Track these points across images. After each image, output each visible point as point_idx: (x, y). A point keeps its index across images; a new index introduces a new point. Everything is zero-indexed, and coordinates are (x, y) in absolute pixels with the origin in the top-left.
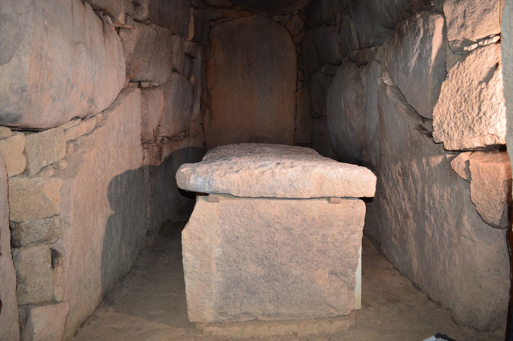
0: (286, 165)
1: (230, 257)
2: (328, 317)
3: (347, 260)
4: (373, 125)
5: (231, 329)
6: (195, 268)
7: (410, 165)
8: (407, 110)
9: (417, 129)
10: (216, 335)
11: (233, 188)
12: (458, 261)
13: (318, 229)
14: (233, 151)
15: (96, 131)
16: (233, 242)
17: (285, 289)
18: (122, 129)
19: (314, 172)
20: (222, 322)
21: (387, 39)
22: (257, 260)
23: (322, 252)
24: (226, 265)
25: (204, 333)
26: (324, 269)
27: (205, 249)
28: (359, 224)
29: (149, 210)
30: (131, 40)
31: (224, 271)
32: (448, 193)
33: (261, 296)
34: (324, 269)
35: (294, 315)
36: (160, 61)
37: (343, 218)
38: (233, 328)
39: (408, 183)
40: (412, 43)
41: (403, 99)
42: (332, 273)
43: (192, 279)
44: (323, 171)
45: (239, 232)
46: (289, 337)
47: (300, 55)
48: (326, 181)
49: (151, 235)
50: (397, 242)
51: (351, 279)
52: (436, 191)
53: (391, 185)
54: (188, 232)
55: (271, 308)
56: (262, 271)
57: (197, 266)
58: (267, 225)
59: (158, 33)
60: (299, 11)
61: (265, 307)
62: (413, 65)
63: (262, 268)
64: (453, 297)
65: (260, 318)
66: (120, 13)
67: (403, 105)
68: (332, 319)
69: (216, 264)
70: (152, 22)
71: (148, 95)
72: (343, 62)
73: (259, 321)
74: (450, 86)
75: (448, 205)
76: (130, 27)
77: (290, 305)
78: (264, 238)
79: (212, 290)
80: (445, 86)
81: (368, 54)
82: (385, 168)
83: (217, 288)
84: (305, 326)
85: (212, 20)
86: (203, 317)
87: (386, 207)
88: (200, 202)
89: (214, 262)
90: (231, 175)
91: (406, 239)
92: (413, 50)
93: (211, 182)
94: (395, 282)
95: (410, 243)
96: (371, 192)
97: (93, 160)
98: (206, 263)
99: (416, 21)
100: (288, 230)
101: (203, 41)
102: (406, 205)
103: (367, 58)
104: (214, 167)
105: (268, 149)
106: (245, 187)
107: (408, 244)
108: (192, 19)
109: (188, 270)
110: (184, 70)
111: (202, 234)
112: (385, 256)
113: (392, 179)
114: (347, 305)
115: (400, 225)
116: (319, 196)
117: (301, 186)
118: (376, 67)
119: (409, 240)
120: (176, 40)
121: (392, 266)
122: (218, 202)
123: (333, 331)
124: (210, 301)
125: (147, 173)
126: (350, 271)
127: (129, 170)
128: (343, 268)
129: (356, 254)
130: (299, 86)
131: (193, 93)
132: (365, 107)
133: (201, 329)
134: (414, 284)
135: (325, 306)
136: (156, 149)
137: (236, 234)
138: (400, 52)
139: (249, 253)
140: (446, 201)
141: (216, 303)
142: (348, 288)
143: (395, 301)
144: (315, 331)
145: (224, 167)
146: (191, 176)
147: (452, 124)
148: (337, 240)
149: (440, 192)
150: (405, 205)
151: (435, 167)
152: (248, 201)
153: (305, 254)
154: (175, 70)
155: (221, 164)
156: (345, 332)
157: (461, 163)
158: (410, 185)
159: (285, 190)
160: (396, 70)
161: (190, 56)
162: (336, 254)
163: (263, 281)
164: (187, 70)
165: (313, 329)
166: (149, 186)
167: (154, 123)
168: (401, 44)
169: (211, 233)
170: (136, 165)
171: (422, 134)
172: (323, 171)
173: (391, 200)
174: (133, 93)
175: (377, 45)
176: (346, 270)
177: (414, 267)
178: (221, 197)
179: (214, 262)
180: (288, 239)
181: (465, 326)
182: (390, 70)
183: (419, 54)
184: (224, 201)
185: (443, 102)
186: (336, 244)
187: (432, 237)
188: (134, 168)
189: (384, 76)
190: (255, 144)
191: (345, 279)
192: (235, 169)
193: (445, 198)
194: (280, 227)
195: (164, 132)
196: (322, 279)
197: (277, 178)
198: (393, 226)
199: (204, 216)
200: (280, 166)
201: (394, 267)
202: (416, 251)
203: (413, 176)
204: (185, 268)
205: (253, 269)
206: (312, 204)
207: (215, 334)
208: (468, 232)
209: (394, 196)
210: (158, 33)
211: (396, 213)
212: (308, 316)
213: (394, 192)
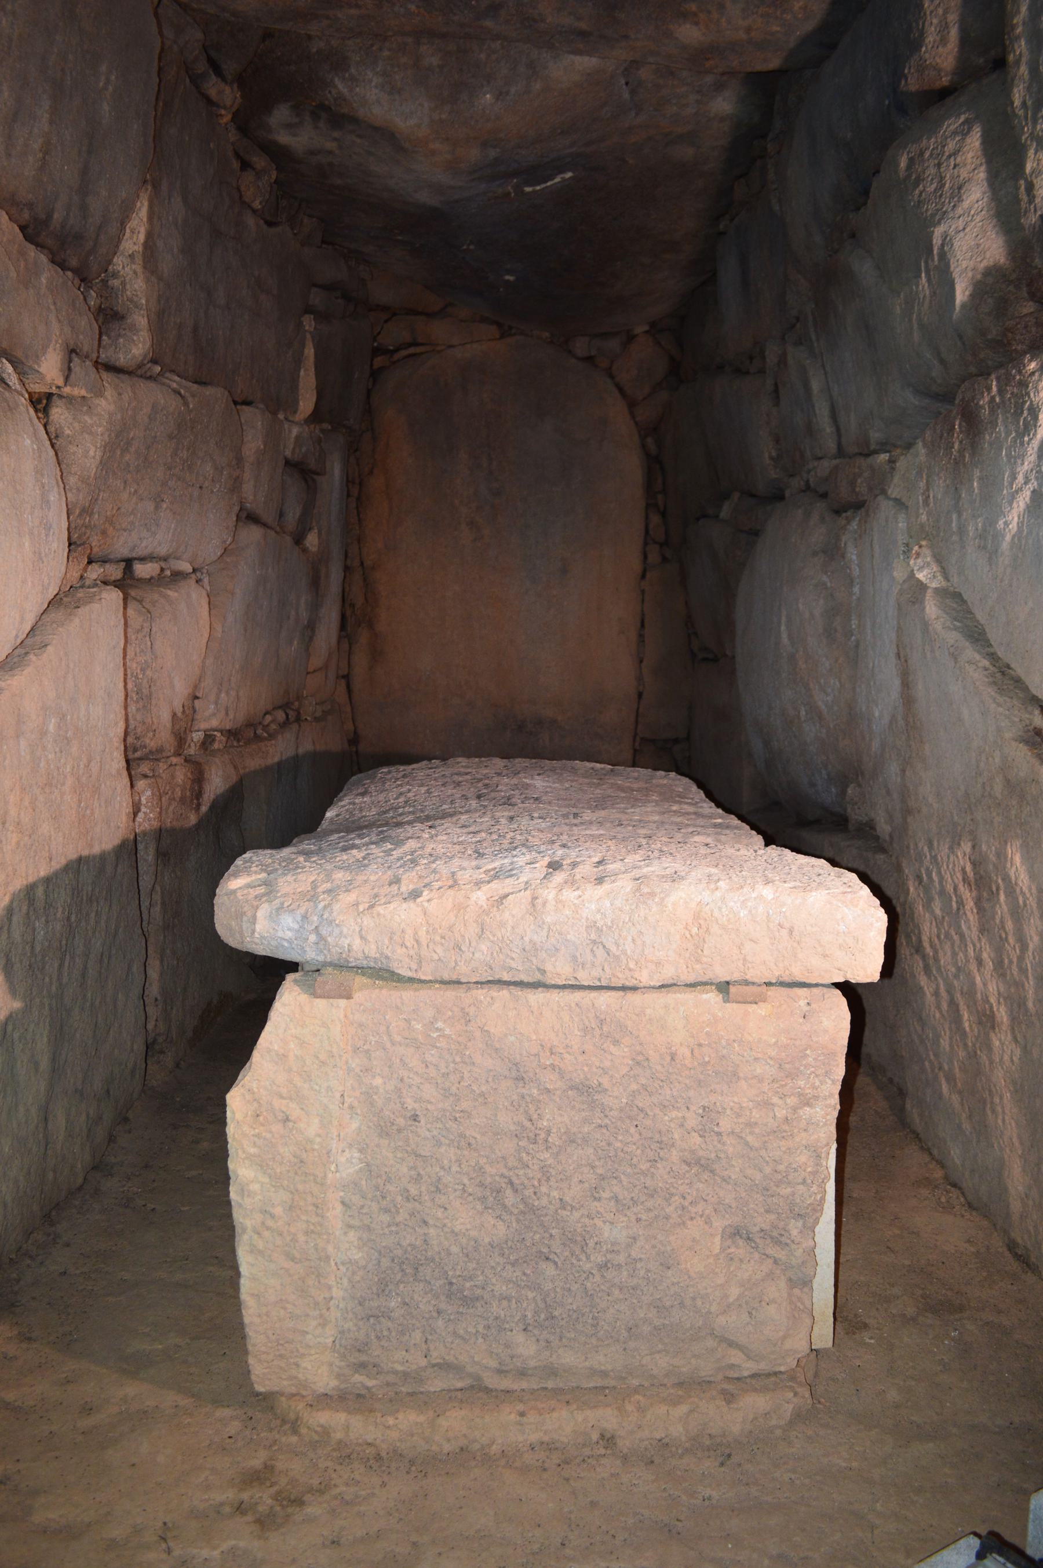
0: (580, 871)
1: (389, 1180)
2: (720, 1377)
3: (787, 1191)
4: (882, 706)
5: (391, 1421)
6: (272, 1216)
7: (1001, 855)
8: (993, 675)
9: (1026, 742)
10: (340, 1442)
11: (400, 951)
13: (688, 1088)
14: (423, 789)
16: (399, 1131)
17: (575, 1287)
18: (51, 728)
19: (672, 898)
20: (363, 1392)
21: (928, 434)
24: (374, 1206)
25: (303, 1431)
26: (708, 1222)
27: (304, 1155)
28: (827, 1074)
29: (154, 974)
30: (91, 433)
31: (369, 1229)
33: (495, 1309)
34: (708, 1222)
35: (604, 1374)
36: (196, 493)
38: (401, 1416)
39: (994, 913)
40: (1009, 456)
41: (978, 636)
42: (735, 1233)
43: (261, 1253)
45: (418, 1100)
46: (587, 1451)
47: (654, 464)
48: (715, 929)
49: (162, 1052)
50: (955, 1099)
51: (799, 1253)
53: (938, 912)
54: (248, 1097)
55: (527, 1348)
56: (496, 1229)
57: (278, 1211)
58: (514, 1074)
59: (186, 404)
60: (653, 325)
61: (507, 1346)
62: (1013, 526)
63: (499, 1217)
65: (492, 1381)
66: (45, 349)
67: (977, 657)
68: (732, 1387)
69: (343, 1203)
70: (167, 369)
71: (154, 603)
72: (787, 493)
73: (488, 1391)
76: (83, 393)
77: (594, 1341)
78: (506, 1120)
79: (330, 1288)
81: (866, 474)
82: (920, 857)
83: (345, 1281)
84: (641, 1410)
85: (377, 351)
86: (300, 1376)
87: (923, 980)
88: (289, 999)
89: (334, 1198)
90: (392, 906)
91: (986, 1095)
92: (1014, 477)
93: (324, 932)
94: (948, 1234)
95: (999, 1109)
96: (867, 968)
98: (309, 1199)
99: (1023, 384)
100: (585, 1091)
101: (350, 416)
102: (988, 985)
103: (862, 487)
104: (339, 876)
105: (539, 783)
106: (439, 950)
107: (993, 1111)
108: (310, 351)
109: (248, 1223)
110: (281, 515)
111: (295, 1103)
112: (917, 1136)
113: (942, 892)
114: (784, 1338)
115: (965, 1045)
116: (691, 979)
117: (629, 947)
118: (890, 523)
119: (997, 1100)
120: (254, 423)
121: (938, 1174)
122: (349, 997)
123: (736, 1429)
125: (148, 855)
126: (795, 1228)
127: (80, 859)
128: (773, 1217)
129: (814, 1173)
130: (650, 559)
131: (316, 583)
132: (857, 646)
133: (292, 1416)
134: (1012, 1246)
135: (710, 1343)
136: (181, 775)
137: (410, 1104)
138: (971, 481)
139: (455, 1168)
141: (342, 1332)
142: (790, 1280)
143: (944, 1307)
144: (677, 1431)
145: (373, 878)
146: (263, 903)
148: (750, 1125)
150: (985, 985)
152: (450, 994)
153: (644, 1174)
154: (249, 517)
155: (361, 865)
158: (1002, 922)
159: (574, 958)
160: (955, 538)
161: (303, 471)
162: (749, 1172)
163: (502, 1260)
164: (293, 514)
165: (671, 1421)
166: (157, 897)
167: (174, 692)
168: (973, 455)
170: (106, 838)
172: (706, 896)
173: (936, 960)
174: (96, 606)
175: (895, 446)
176: (781, 1224)
177: (1012, 1191)
178: (360, 980)
179: (334, 1198)
180: (585, 1121)
182: (935, 537)
183: (1034, 492)
184: (367, 995)
186: (750, 1138)
188: (96, 850)
189: (918, 555)
190: (499, 763)
192: (406, 887)
194: (559, 1084)
195: (212, 717)
196: (701, 1258)
197: (548, 919)
198: (945, 1043)
200: (559, 877)
201: (946, 1177)
202: (1020, 1138)
203: (1011, 892)
204: (237, 1215)
205: (465, 1220)
206: (666, 1007)
207: (339, 1435)
209: (947, 947)
210: (186, 404)
211: (953, 1003)
212: (654, 1377)
213: (947, 935)
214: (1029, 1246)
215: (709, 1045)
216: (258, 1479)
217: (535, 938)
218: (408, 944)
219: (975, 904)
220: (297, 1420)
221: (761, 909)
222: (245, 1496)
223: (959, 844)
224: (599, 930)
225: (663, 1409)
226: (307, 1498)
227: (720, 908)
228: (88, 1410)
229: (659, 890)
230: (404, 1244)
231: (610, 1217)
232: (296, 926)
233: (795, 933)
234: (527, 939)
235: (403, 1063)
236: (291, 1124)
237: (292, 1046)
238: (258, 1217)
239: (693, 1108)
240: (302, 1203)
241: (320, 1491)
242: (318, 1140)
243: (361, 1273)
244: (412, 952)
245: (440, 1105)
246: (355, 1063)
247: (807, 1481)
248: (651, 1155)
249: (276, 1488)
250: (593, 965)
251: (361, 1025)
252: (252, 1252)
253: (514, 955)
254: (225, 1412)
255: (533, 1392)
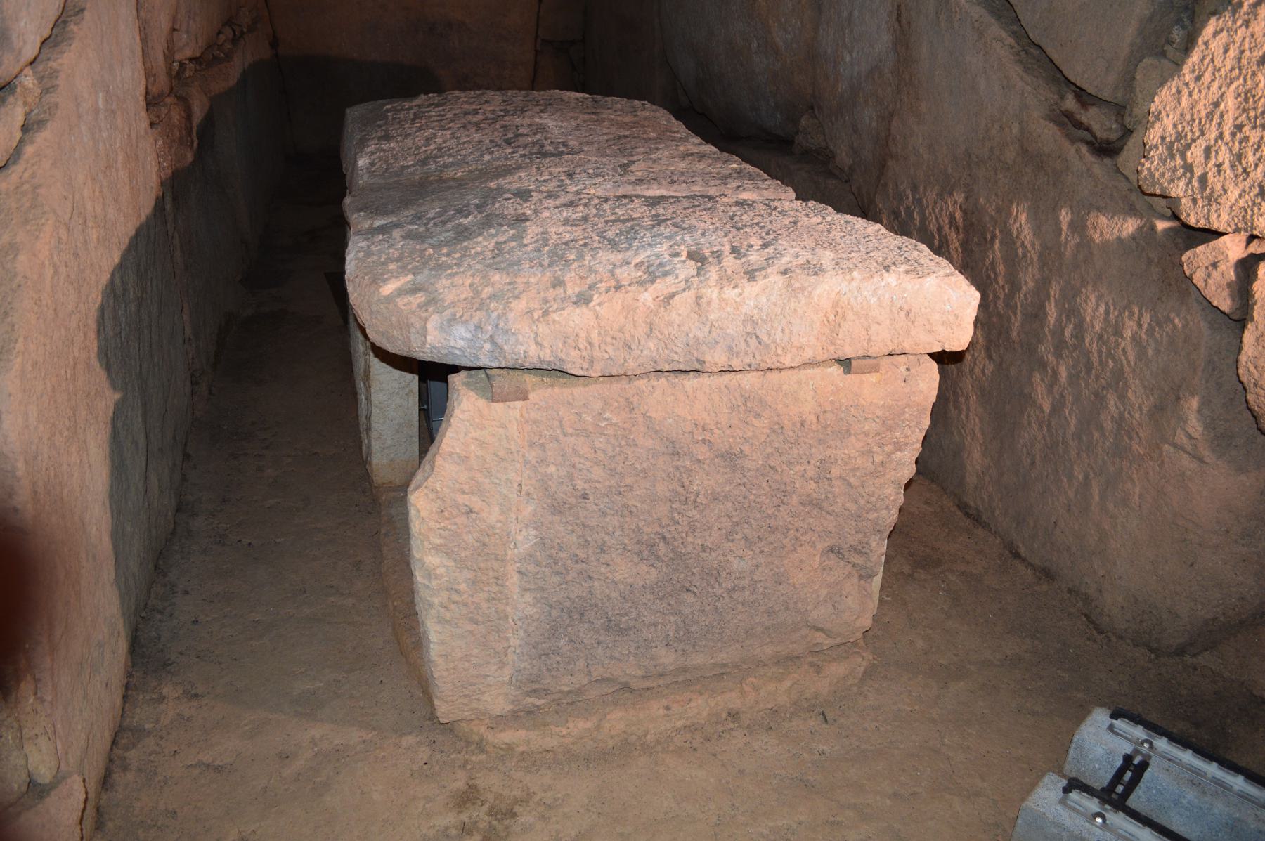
1: (561, 548)
6: (458, 592)
7: (1004, 212)
8: (1018, 54)
9: (1051, 120)
11: (574, 353)
12: (1137, 498)
15: (29, 150)
16: (570, 508)
17: (708, 608)
19: (818, 291)
22: (637, 548)
23: (815, 504)
25: (489, 749)
27: (487, 540)
32: (1140, 326)
33: (645, 634)
35: (725, 665)
37: (880, 413)
38: (571, 725)
42: (835, 550)
44: (844, 287)
45: (589, 481)
46: (720, 728)
48: (850, 316)
52: (1094, 308)
54: (432, 496)
55: (667, 658)
57: (463, 587)
58: (671, 450)
64: (1102, 572)
67: (1004, 34)
69: (520, 572)
74: (1238, 38)
75: (1132, 355)
78: (662, 489)
80: (1216, 34)
83: (521, 633)
84: (756, 689)
86: (481, 707)
89: (512, 568)
90: (565, 313)
93: (499, 341)
96: (960, 337)
97: (49, 272)
100: (730, 458)
107: (957, 407)
109: (436, 600)
119: (962, 400)
122: (525, 398)
124: (502, 665)
128: (860, 536)
133: (476, 738)
135: (805, 631)
139: (618, 533)
140: (1126, 343)
144: (783, 700)
147: (1224, 156)
148: (854, 470)
149: (1107, 313)
151: (1105, 245)
153: (769, 517)
156: (855, 689)
157: (1222, 267)
159: (730, 348)
163: (652, 597)
165: (779, 691)
169: (505, 492)
171: (1073, 141)
172: (844, 287)
177: (969, 468)
179: (512, 568)
180: (729, 482)
181: (1121, 638)
184: (542, 394)
185: (1198, 78)
186: (852, 480)
187: (1050, 415)
191: (859, 560)
192: (573, 289)
193: (1128, 334)
197: (712, 317)
199: (482, 444)
205: (624, 570)
206: (799, 382)
207: (521, 749)
208: (1190, 437)
214: (981, 508)
215: (832, 411)
216: (468, 799)
217: (699, 334)
218: (581, 346)
219: (961, 245)
220: (481, 741)
221: (887, 296)
222: (464, 817)
223: (951, 194)
224: (755, 323)
225: (772, 687)
226: (517, 809)
227: (856, 298)
228: (285, 757)
229: (806, 284)
230: (572, 596)
231: (739, 553)
232: (469, 336)
233: (912, 315)
234: (691, 335)
235: (576, 452)
236: (474, 516)
237: (473, 447)
238: (444, 594)
239: (813, 462)
240: (484, 578)
241: (524, 801)
242: (499, 525)
243: (535, 624)
244: (584, 354)
245: (607, 483)
246: (532, 455)
247: (889, 727)
248: (776, 501)
249: (487, 805)
250: (746, 353)
251: (536, 422)
252: (439, 622)
253: (678, 350)
254: (408, 740)
255: (667, 686)
